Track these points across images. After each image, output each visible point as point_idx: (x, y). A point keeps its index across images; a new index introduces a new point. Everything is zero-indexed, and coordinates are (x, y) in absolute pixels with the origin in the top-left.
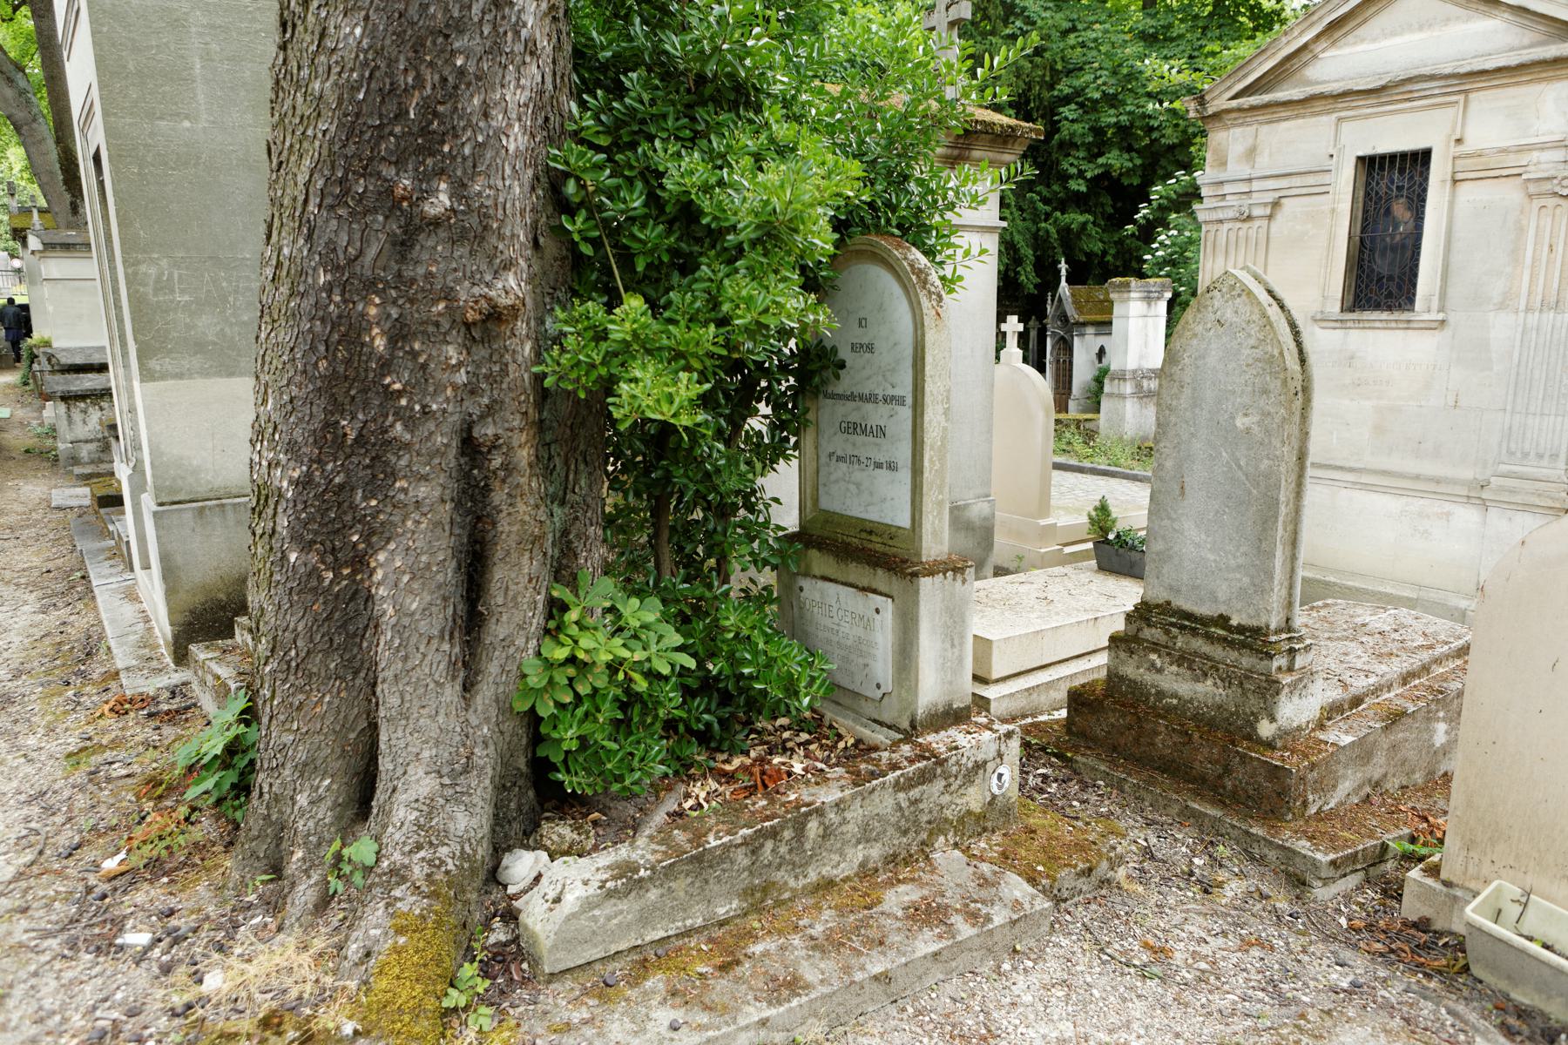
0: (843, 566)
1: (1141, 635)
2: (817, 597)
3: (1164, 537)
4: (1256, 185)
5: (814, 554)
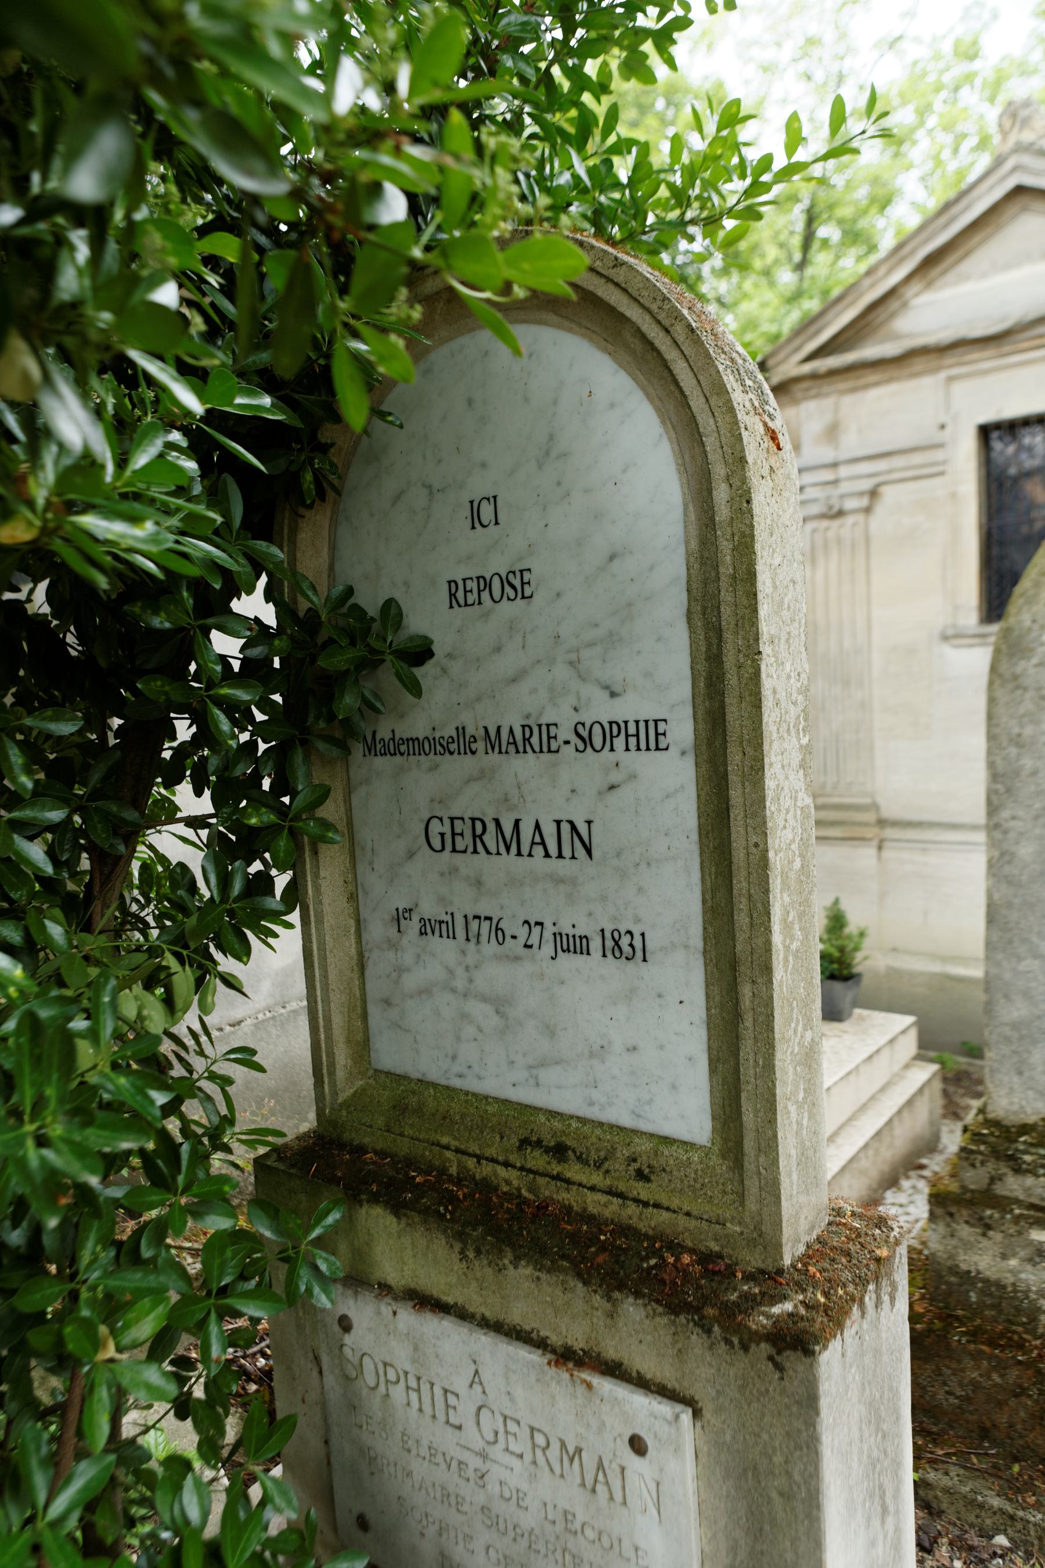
0: (483, 1270)
1: (999, 1189)
2: (401, 1356)
3: (1027, 994)
4: (844, 471)
5: (377, 1219)
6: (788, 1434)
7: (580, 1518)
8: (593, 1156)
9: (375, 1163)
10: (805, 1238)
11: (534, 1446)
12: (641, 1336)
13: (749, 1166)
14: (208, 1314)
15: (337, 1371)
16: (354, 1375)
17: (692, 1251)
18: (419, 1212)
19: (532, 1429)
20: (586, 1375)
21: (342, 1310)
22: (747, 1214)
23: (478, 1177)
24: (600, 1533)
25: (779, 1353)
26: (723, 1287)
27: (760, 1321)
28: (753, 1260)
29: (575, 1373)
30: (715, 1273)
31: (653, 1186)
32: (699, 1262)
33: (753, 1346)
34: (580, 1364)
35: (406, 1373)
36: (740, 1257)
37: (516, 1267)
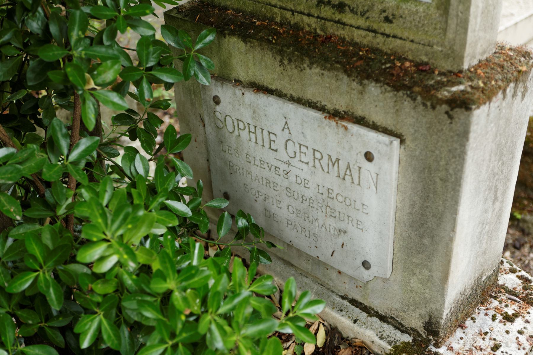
2: (246, 116)
5: (234, 45)
6: (450, 151)
7: (336, 192)
8: (360, 9)
9: (233, 15)
10: (479, 57)
11: (315, 158)
12: (376, 103)
13: (452, 12)
14: (142, 78)
15: (212, 125)
16: (222, 127)
17: (411, 61)
18: (257, 40)
19: (314, 150)
20: (345, 123)
21: (215, 93)
22: (447, 40)
23: (292, 23)
24: (345, 198)
25: (452, 110)
26: (426, 78)
27: (444, 94)
28: (446, 65)
29: (339, 122)
30: (422, 71)
31: (393, 25)
32: (414, 66)
33: (438, 107)
34: (342, 118)
35: (249, 124)
36: (439, 64)
37: (310, 69)
